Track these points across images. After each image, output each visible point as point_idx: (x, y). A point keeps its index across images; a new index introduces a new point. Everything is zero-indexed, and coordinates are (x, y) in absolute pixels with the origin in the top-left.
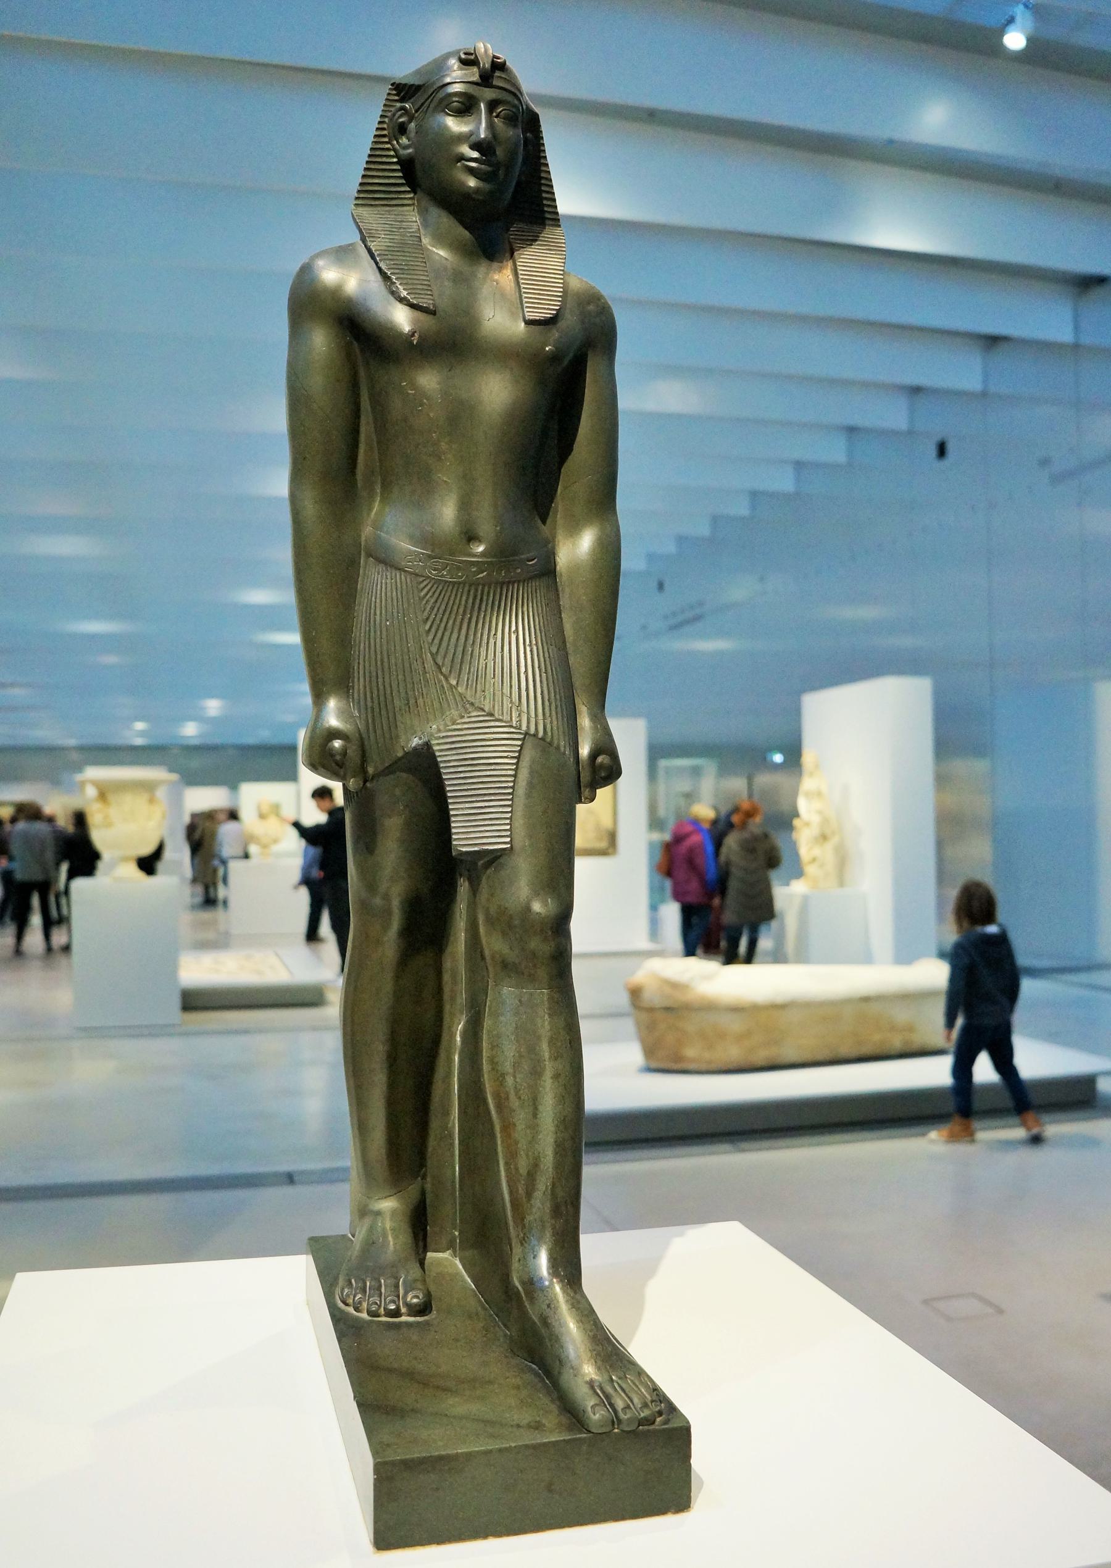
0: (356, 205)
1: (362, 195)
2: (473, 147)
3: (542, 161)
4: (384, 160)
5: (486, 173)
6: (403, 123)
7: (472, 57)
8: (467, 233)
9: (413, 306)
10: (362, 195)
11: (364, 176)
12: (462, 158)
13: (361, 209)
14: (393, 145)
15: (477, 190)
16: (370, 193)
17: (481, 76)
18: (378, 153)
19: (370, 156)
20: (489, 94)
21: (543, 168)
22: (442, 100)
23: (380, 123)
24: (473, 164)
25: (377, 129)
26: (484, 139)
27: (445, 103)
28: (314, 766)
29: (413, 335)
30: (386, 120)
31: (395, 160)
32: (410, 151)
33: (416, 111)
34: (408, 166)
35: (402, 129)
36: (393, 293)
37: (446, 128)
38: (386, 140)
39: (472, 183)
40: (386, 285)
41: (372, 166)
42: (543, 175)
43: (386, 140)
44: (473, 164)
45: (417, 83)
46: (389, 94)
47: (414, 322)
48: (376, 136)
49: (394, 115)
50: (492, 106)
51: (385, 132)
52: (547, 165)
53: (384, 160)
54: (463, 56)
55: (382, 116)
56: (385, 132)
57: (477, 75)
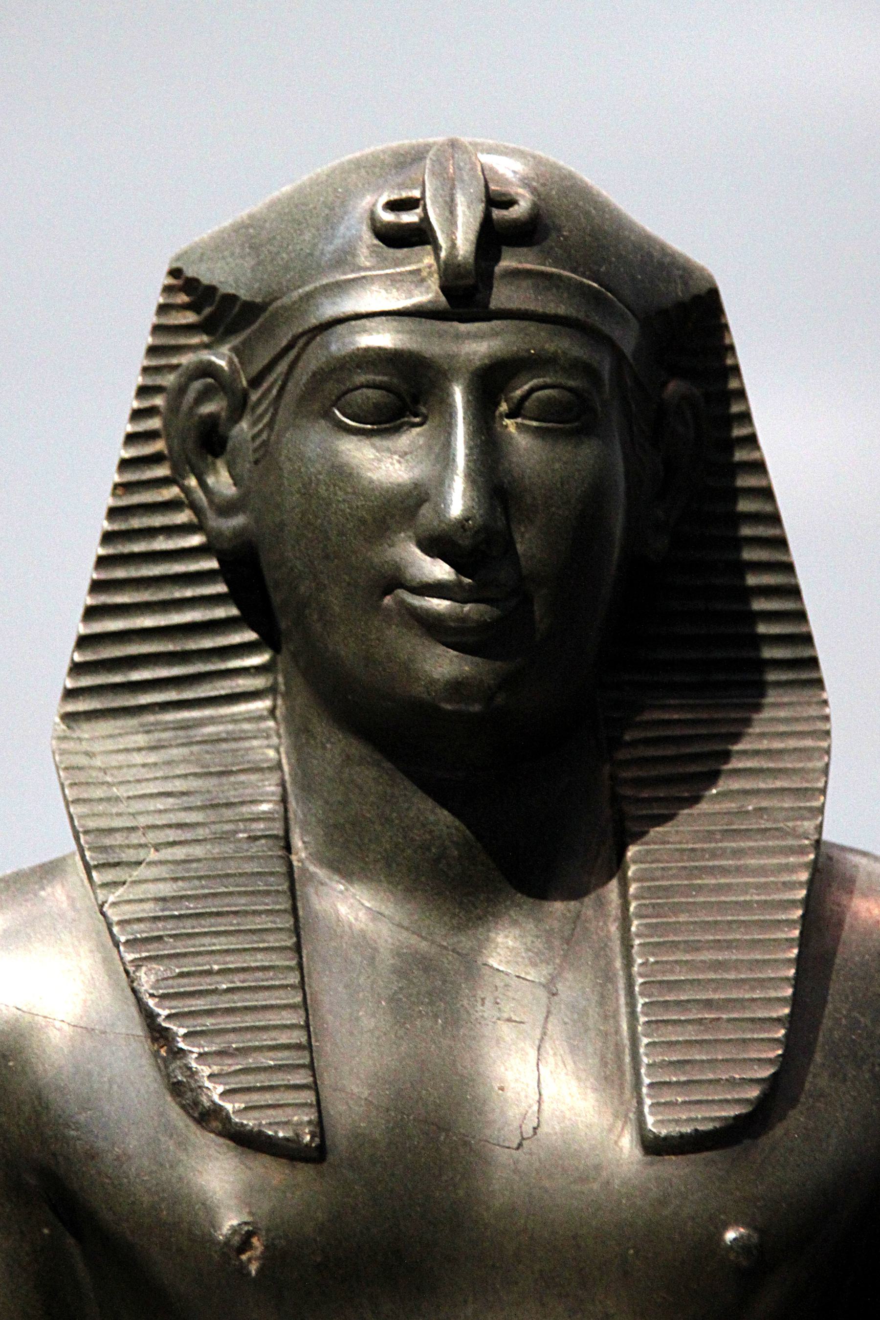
0: (69, 718)
1: (87, 681)
2: (435, 546)
3: (738, 432)
4: (161, 544)
5: (483, 627)
6: (212, 420)
7: (410, 217)
8: (444, 816)
9: (247, 1141)
10: (87, 681)
11: (97, 587)
12: (395, 580)
13: (86, 730)
14: (186, 490)
15: (457, 687)
16: (112, 674)
17: (444, 289)
18: (136, 523)
19: (108, 538)
20: (477, 344)
21: (740, 455)
22: (320, 377)
23: (137, 415)
24: (439, 605)
25: (131, 439)
26: (462, 524)
27: (332, 388)
28: (645, 1036)
29: (245, 1244)
30: (159, 401)
31: (196, 540)
32: (238, 521)
33: (255, 382)
34: (245, 572)
35: (210, 441)
36: (177, 1089)
37: (343, 474)
38: (162, 471)
39: (443, 664)
40: (156, 1055)
41: (120, 573)
42: (745, 506)
43: (162, 471)
44: (439, 605)
45: (244, 294)
46: (163, 309)
47: (248, 1196)
48: (125, 464)
49: (182, 390)
50: (491, 384)
51: (159, 446)
52: (760, 467)
53: (161, 544)
54: (388, 217)
55: (143, 391)
56: (159, 446)
57: (434, 283)
